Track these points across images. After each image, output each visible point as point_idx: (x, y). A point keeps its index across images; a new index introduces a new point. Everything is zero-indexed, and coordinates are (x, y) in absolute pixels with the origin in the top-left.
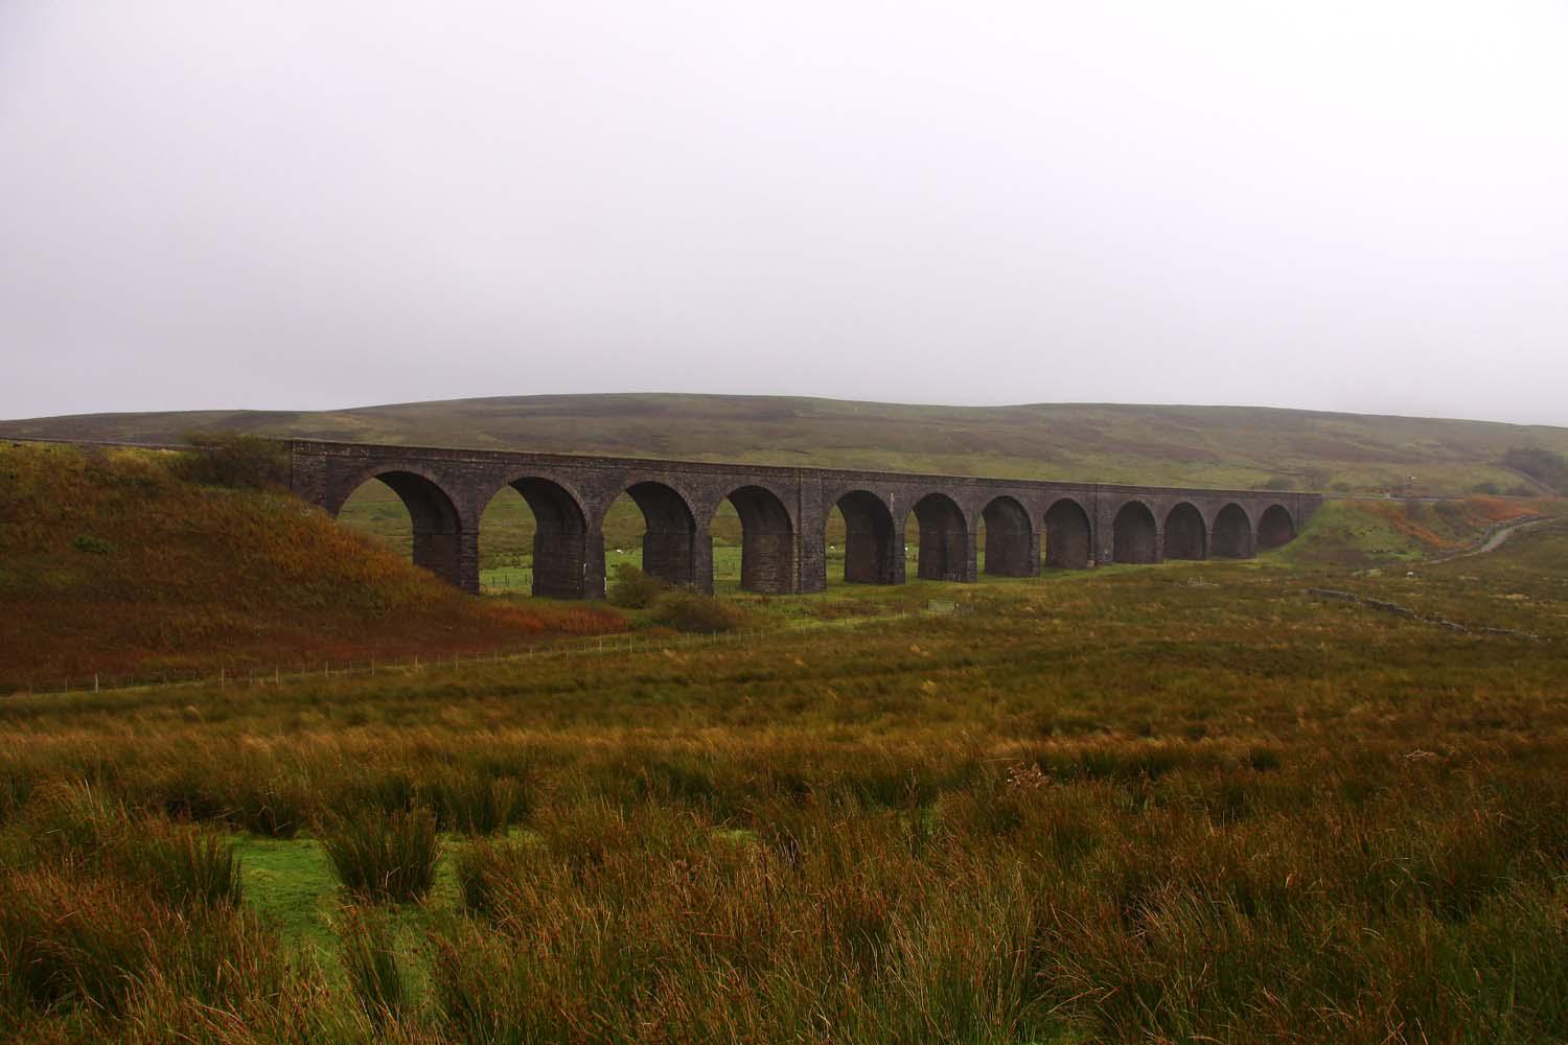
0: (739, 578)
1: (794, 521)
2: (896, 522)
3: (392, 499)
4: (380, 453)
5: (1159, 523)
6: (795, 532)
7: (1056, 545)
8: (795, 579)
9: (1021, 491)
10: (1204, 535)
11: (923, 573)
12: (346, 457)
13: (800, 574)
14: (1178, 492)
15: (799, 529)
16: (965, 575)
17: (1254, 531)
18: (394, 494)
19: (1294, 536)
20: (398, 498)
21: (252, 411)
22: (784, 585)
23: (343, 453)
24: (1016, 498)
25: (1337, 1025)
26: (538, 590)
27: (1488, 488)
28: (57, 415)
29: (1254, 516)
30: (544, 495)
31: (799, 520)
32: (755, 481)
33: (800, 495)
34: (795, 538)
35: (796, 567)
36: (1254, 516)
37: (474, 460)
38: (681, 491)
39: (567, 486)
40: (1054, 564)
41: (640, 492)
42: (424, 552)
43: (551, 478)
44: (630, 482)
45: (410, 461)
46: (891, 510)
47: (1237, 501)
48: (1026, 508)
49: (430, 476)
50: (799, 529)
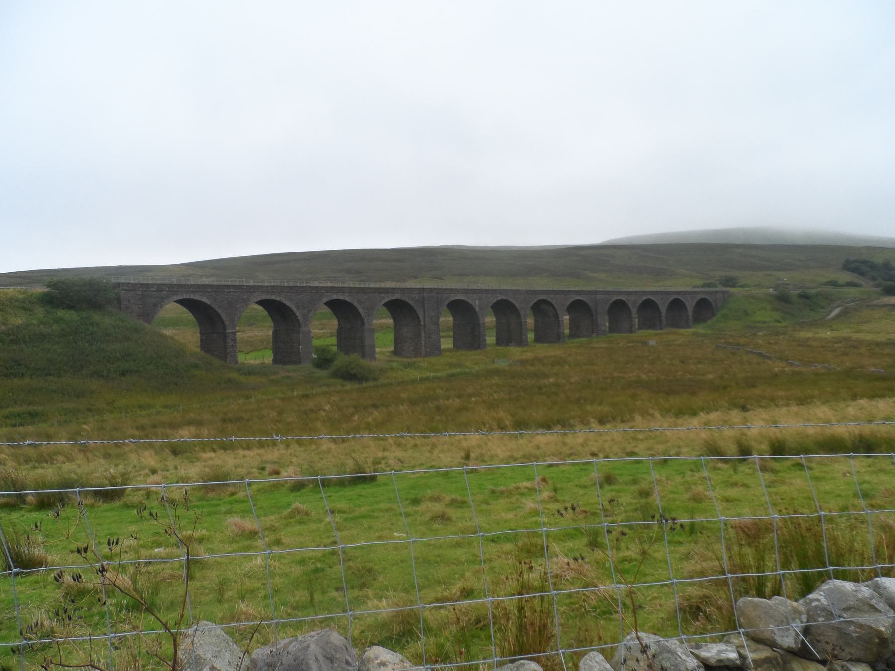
0: (393, 349)
1: (421, 318)
2: (480, 316)
3: (185, 313)
4: (173, 288)
5: (634, 311)
6: (422, 323)
7: (574, 325)
8: (423, 350)
9: (552, 296)
10: (660, 316)
11: (499, 343)
12: (154, 291)
13: (425, 347)
14: (645, 293)
15: (424, 321)
16: (521, 342)
17: (690, 313)
18: (191, 314)
19: (714, 315)
20: (187, 311)
21: (251, 256)
22: (417, 353)
23: (152, 289)
24: (549, 300)
25: (796, 526)
26: (276, 361)
27: (834, 284)
28: (512, 245)
29: (690, 304)
30: (340, 307)
31: (424, 318)
32: (397, 296)
33: (424, 303)
34: (422, 327)
35: (423, 343)
36: (690, 304)
37: (232, 290)
38: (355, 304)
39: (288, 304)
40: (573, 335)
41: (335, 305)
42: (206, 345)
43: (278, 299)
44: (325, 300)
45: (194, 292)
46: (477, 309)
47: (679, 297)
48: (555, 305)
49: (205, 300)
50: (424, 321)
